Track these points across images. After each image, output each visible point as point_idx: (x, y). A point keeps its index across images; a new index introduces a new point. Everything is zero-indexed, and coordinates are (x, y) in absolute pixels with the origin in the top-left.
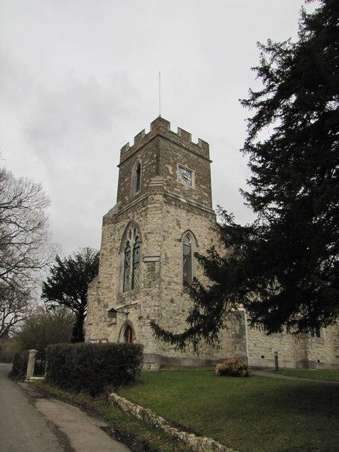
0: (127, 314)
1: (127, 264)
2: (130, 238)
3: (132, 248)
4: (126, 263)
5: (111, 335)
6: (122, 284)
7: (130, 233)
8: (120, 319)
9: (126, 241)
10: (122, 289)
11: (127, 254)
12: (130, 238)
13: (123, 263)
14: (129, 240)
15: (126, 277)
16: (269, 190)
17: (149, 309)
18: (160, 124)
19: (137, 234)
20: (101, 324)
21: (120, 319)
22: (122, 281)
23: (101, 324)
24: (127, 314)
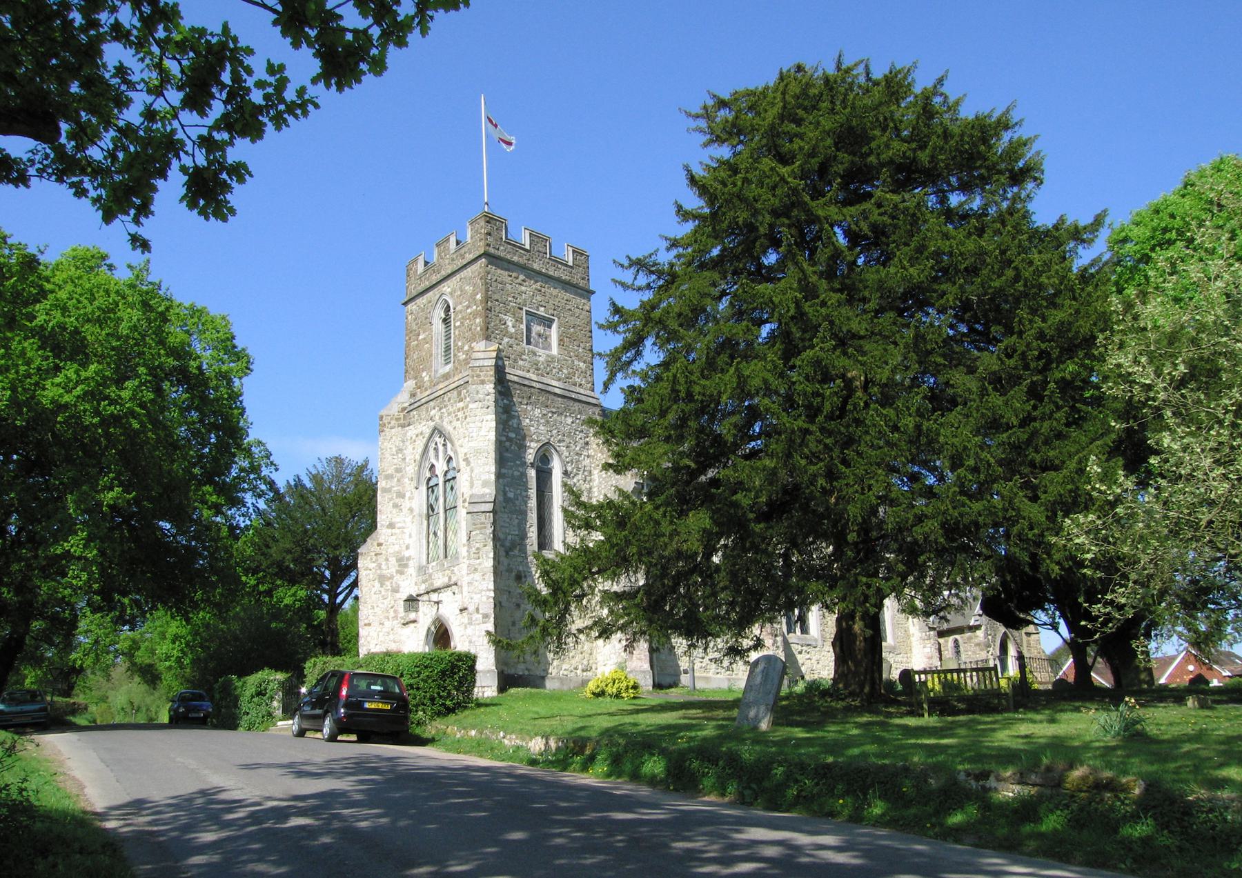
1: (433, 510)
4: (431, 507)
7: (436, 449)
9: (428, 465)
10: (425, 557)
11: (431, 489)
13: (425, 507)
15: (430, 534)
20: (387, 624)
23: (387, 624)
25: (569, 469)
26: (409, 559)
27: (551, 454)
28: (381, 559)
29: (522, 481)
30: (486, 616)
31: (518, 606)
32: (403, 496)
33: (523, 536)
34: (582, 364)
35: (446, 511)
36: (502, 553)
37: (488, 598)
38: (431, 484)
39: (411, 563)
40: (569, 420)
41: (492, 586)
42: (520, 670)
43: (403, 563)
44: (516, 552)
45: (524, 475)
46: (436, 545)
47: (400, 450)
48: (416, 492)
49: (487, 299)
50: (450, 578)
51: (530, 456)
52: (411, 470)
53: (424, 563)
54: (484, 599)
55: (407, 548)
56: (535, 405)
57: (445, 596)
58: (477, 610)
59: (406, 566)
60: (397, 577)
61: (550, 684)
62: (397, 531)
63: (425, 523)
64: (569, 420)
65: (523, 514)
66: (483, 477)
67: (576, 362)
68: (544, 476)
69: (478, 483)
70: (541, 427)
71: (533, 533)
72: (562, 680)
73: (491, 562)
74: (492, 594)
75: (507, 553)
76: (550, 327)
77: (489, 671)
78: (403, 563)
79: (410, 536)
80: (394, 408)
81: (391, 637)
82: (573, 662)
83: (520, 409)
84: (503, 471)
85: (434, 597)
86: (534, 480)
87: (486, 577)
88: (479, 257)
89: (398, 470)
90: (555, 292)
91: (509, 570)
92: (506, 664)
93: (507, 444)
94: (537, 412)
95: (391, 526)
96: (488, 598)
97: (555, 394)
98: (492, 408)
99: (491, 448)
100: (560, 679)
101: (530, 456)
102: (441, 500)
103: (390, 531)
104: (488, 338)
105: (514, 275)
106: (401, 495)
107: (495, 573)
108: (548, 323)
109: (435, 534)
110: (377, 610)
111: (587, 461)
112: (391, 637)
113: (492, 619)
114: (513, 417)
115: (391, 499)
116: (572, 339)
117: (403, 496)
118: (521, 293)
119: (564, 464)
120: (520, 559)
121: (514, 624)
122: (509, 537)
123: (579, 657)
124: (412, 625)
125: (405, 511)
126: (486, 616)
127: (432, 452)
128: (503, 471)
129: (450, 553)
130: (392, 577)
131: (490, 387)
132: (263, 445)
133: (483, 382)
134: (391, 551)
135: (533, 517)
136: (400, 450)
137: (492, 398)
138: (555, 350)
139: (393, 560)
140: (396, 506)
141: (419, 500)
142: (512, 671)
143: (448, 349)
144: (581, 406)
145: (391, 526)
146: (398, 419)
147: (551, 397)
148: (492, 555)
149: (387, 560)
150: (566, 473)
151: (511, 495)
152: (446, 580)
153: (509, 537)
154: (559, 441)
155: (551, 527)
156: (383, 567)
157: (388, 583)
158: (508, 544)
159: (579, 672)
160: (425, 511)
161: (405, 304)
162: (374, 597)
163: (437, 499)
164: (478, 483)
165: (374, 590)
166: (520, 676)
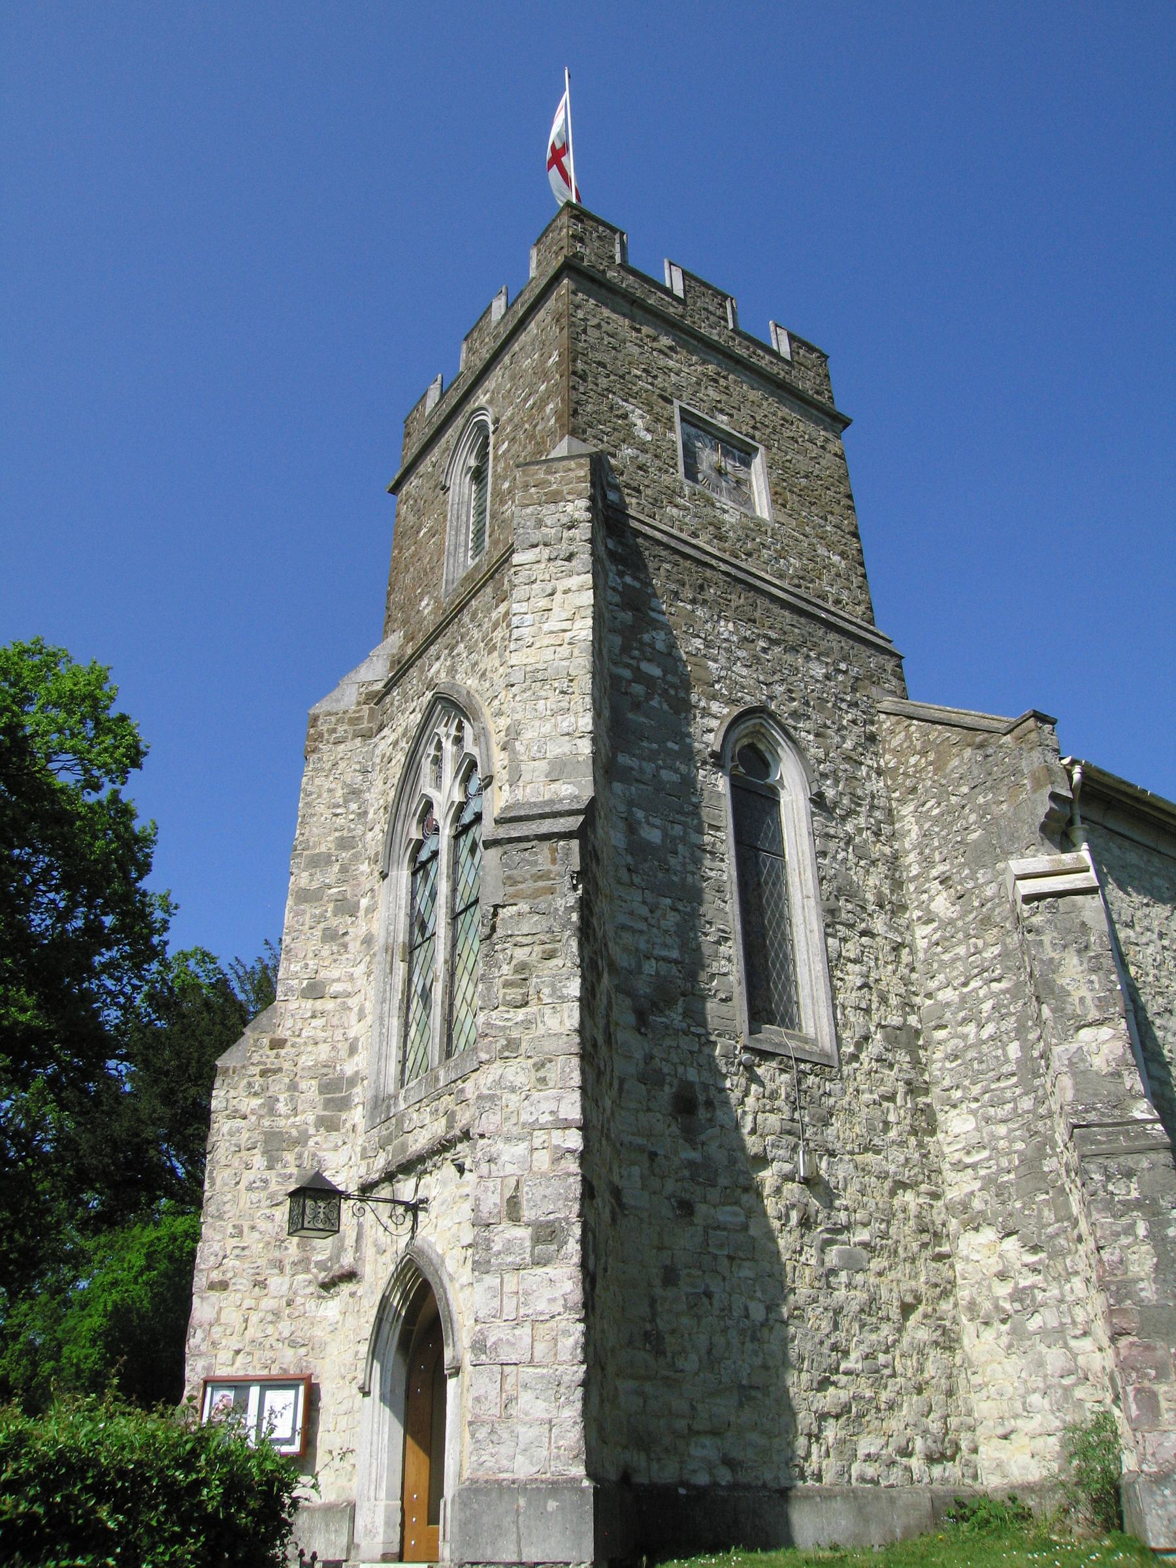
0: (414, 1208)
1: (423, 927)
2: (438, 786)
3: (446, 832)
4: (419, 924)
5: (333, 1350)
6: (395, 1041)
7: (437, 761)
8: (373, 1244)
9: (416, 805)
10: (393, 1068)
11: (420, 868)
12: (438, 786)
13: (403, 922)
14: (430, 791)
15: (414, 997)
16: (635, 578)
17: (522, 1148)
18: (137, 817)
19: (469, 747)
20: (278, 1283)
21: (373, 1244)
22: (395, 1023)
23: (278, 1283)
24: (414, 1208)
25: (830, 793)
26: (352, 1082)
27: (773, 746)
28: (278, 1086)
29: (683, 801)
30: (547, 1233)
31: (686, 1208)
32: (353, 911)
33: (692, 963)
34: (836, 559)
35: (454, 917)
36: (625, 1016)
37: (560, 1155)
38: (424, 855)
39: (359, 1094)
40: (819, 671)
41: (572, 1109)
42: (700, 1464)
43: (336, 1093)
44: (675, 1017)
45: (688, 784)
46: (424, 1026)
47: (354, 793)
48: (382, 888)
49: (573, 355)
50: (451, 1117)
51: (709, 730)
52: (374, 839)
53: (391, 1089)
54: (542, 1160)
55: (353, 1050)
56: (719, 610)
57: (438, 1185)
58: (513, 1207)
59: (344, 1104)
60: (318, 1140)
61: (810, 1526)
62: (329, 1005)
63: (401, 968)
64: (819, 671)
65: (689, 896)
66: (555, 750)
67: (822, 551)
68: (756, 806)
69: (536, 771)
70: (738, 668)
71: (727, 966)
72: (862, 1499)
73: (570, 1017)
74: (574, 1140)
75: (641, 1016)
76: (747, 464)
77: (555, 1487)
78: (336, 1093)
79: (361, 1017)
80: (348, 696)
81: (285, 1327)
82: (893, 1424)
83: (674, 610)
84: (623, 759)
85: (406, 1189)
86: (727, 805)
87: (552, 1072)
88: (555, 279)
89: (345, 843)
90: (755, 395)
91: (651, 1078)
92: (642, 1441)
93: (638, 689)
94: (726, 628)
95: (315, 990)
96: (560, 1155)
97: (774, 599)
98: (584, 558)
99: (581, 664)
100: (852, 1496)
101: (709, 730)
102: (444, 888)
103: (309, 1004)
104: (575, 432)
105: (645, 330)
106: (346, 907)
107: (589, 1055)
108: (745, 454)
109: (426, 996)
110: (250, 1238)
111: (877, 785)
112: (285, 1327)
113: (573, 1247)
114: (655, 625)
115: (322, 918)
116: (808, 498)
117: (353, 911)
118: (666, 371)
119: (814, 776)
120: (685, 1043)
121: (670, 1277)
122: (650, 967)
123: (910, 1407)
124: (346, 1288)
125: (354, 946)
126: (547, 1233)
127: (427, 766)
128: (623, 759)
129: (460, 1043)
130: (302, 1140)
131: (578, 508)
132: (213, 960)
133: (555, 498)
134: (306, 1061)
135: (724, 911)
136: (354, 793)
137: (583, 532)
138: (763, 509)
139: (310, 1088)
140: (330, 936)
141: (385, 907)
142: (665, 1473)
143: (479, 533)
144: (846, 643)
145: (315, 990)
146: (354, 721)
147: (763, 602)
148: (574, 988)
149: (293, 1087)
150: (818, 800)
151: (654, 836)
152: (438, 1128)
153: (650, 967)
154: (794, 714)
155: (789, 982)
156: (281, 1107)
157: (289, 1157)
158: (643, 987)
159: (916, 1463)
160: (402, 937)
161: (395, 489)
162: (246, 1198)
163: (433, 896)
164: (536, 771)
165: (248, 1176)
166: (700, 1494)
